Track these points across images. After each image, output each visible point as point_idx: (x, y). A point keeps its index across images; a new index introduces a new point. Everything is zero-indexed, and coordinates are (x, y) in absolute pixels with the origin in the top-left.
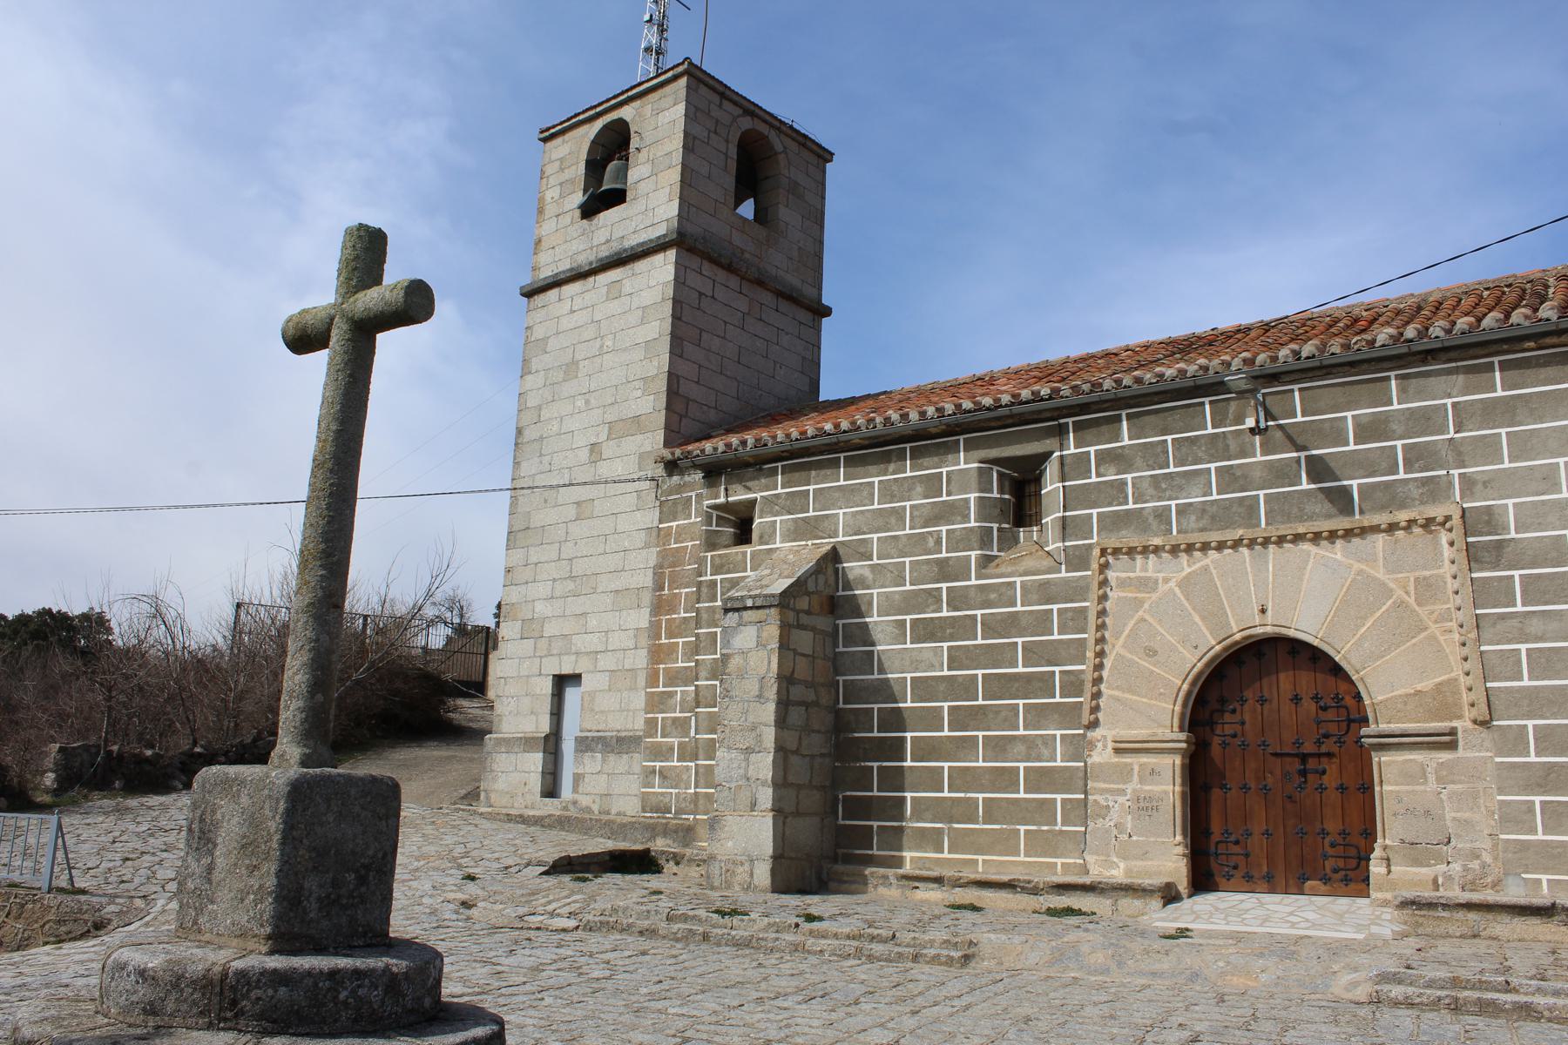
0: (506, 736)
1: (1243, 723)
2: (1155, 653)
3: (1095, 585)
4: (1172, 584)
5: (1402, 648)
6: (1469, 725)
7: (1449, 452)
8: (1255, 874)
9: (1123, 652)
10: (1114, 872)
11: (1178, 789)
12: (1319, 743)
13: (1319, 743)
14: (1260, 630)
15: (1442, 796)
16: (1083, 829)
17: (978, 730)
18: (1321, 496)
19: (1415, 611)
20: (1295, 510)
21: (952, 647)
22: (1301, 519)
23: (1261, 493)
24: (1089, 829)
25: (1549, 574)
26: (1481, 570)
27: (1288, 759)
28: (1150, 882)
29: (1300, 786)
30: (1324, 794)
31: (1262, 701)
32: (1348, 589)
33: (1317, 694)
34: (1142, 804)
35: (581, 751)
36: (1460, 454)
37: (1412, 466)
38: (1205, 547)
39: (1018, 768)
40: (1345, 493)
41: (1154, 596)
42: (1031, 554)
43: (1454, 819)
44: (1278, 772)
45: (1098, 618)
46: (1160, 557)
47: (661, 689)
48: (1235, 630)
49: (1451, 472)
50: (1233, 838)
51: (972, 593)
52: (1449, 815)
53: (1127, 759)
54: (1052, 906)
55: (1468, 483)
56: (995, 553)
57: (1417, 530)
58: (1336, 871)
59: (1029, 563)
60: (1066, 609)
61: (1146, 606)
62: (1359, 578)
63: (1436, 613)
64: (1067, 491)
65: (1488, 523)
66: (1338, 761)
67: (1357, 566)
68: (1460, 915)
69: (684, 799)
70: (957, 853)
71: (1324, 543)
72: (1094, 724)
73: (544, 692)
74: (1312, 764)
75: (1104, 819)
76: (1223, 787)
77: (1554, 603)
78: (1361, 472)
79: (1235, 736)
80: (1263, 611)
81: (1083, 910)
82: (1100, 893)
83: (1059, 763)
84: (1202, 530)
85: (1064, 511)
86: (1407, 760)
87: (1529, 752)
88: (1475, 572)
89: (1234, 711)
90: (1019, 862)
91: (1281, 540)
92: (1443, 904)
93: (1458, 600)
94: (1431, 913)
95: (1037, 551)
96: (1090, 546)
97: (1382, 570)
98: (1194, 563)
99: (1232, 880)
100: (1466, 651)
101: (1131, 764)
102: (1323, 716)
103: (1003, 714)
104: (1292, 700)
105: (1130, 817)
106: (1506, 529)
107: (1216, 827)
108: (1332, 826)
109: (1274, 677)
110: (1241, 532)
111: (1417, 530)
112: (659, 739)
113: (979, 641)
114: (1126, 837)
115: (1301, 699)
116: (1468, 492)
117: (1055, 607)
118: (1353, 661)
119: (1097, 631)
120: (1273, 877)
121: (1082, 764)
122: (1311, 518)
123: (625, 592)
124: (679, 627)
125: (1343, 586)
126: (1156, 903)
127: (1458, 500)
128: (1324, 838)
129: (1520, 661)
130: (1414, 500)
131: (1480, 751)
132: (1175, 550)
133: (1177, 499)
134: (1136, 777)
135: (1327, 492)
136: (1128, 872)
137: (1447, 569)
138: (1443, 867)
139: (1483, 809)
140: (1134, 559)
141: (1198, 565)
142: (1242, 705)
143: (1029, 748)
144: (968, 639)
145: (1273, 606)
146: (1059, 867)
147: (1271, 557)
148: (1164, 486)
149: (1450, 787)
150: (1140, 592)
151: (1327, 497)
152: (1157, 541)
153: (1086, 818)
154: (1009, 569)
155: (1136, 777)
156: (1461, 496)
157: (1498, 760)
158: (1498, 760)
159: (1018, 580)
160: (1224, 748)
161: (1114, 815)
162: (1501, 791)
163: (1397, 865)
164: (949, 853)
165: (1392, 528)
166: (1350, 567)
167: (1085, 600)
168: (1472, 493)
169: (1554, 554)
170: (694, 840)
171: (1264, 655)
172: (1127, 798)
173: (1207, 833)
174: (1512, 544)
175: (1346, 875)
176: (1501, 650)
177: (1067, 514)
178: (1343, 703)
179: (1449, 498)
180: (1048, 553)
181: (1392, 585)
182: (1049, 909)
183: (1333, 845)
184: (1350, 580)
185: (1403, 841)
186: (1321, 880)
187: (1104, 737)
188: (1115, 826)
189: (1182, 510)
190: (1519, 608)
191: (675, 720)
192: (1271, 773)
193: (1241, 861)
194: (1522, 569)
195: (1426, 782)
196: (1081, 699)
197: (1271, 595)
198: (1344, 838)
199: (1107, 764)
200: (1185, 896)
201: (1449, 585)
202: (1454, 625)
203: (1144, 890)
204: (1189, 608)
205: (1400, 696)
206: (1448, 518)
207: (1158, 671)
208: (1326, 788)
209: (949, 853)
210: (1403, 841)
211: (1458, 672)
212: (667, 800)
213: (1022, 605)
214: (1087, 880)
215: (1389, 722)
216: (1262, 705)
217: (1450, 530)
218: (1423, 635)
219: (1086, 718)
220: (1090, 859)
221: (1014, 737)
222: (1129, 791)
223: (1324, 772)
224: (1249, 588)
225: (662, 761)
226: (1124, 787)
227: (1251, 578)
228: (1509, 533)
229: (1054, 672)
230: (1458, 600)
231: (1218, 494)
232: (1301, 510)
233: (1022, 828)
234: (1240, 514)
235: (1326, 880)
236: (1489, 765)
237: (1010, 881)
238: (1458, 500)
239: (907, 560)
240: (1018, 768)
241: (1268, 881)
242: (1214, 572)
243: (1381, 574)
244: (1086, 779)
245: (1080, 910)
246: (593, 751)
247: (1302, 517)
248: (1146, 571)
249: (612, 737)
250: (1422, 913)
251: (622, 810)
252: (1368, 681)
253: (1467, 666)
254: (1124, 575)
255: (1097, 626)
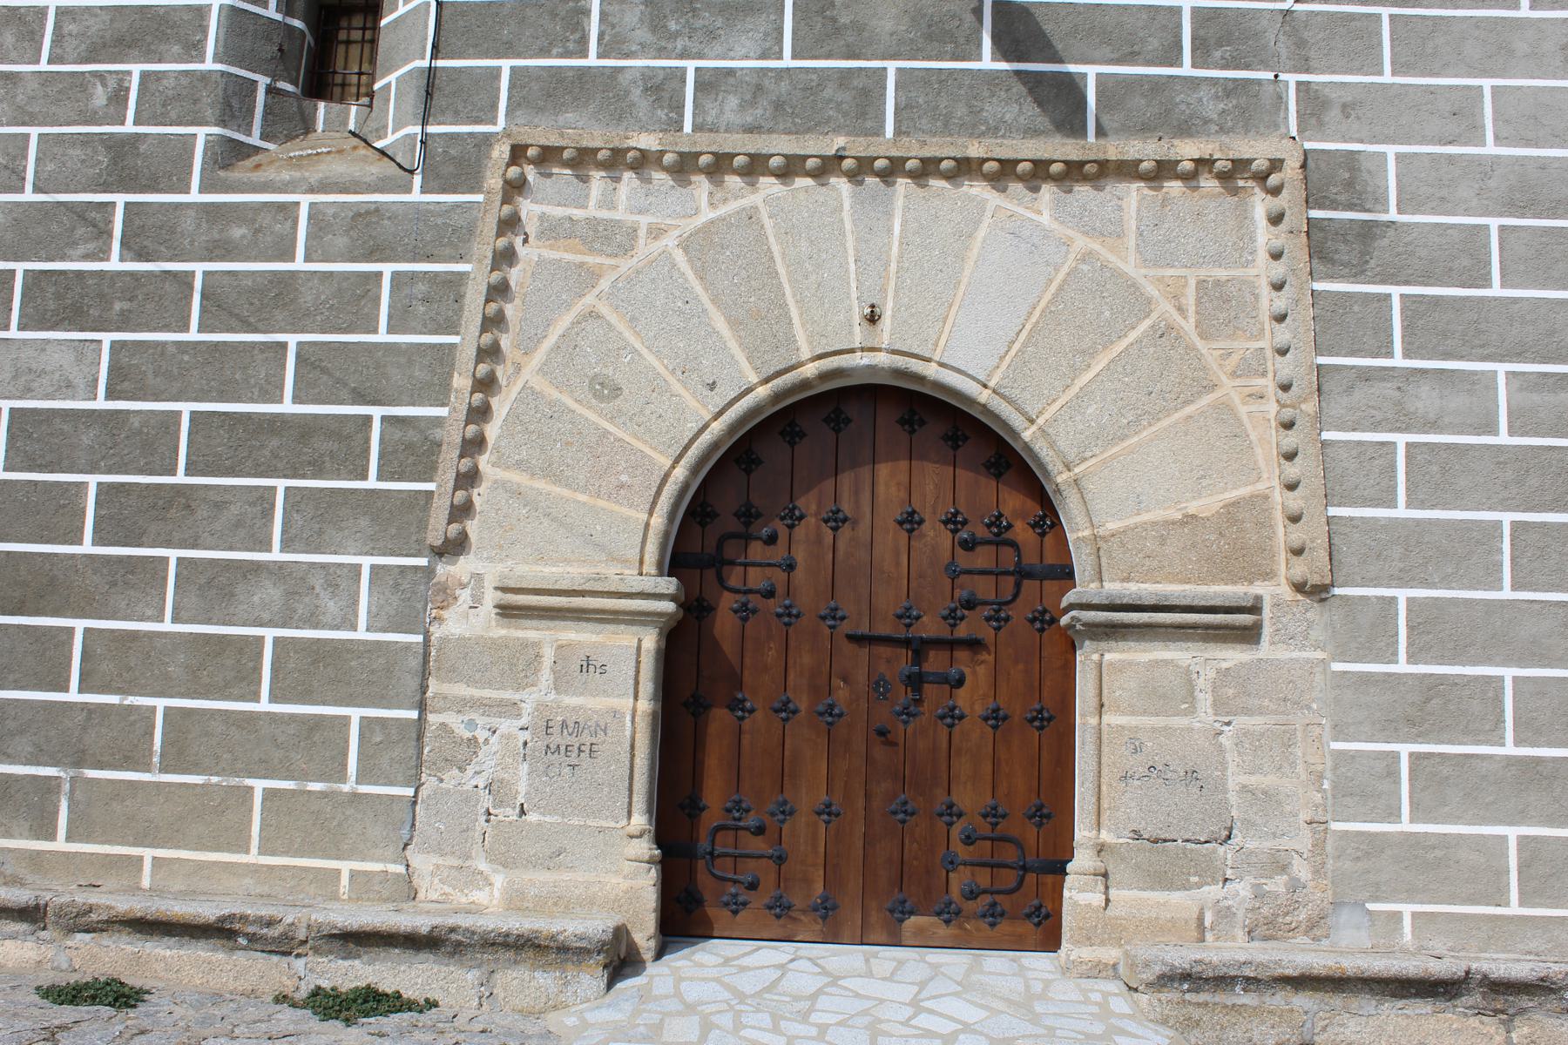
1: (791, 567)
2: (617, 391)
3: (490, 225)
4: (670, 241)
5: (1166, 422)
6: (1287, 593)
7: (1281, 37)
8: (798, 901)
9: (539, 383)
10: (480, 896)
11: (645, 705)
12: (952, 618)
13: (952, 618)
14: (861, 360)
15: (1222, 739)
16: (410, 792)
17: (168, 544)
18: (1019, 88)
19: (1195, 349)
20: (961, 111)
21: (124, 344)
22: (973, 129)
23: (892, 66)
24: (423, 792)
25: (1455, 299)
26: (1331, 277)
27: (884, 651)
28: (580, 930)
29: (906, 711)
30: (956, 729)
31: (836, 520)
32: (1061, 288)
33: (955, 514)
34: (556, 739)
36: (1301, 44)
37: (1208, 53)
38: (755, 167)
39: (261, 639)
40: (1070, 89)
41: (626, 265)
42: (340, 152)
43: (1244, 789)
44: (861, 676)
45: (487, 301)
46: (649, 181)
48: (805, 354)
49: (1282, 77)
50: (751, 821)
51: (188, 223)
52: (1235, 780)
53: (530, 632)
54: (326, 984)
55: (1314, 104)
56: (255, 140)
57: (1208, 183)
58: (972, 895)
59: (338, 168)
60: (413, 276)
61: (604, 284)
62: (1085, 267)
63: (1235, 358)
64: (446, 13)
65: (1350, 184)
66: (991, 658)
67: (1081, 243)
68: (1279, 999)
70: (88, 838)
71: (1016, 187)
72: (455, 547)
74: (935, 662)
75: (462, 769)
76: (735, 705)
77: (1461, 358)
78: (1106, 51)
79: (770, 594)
80: (873, 318)
81: (407, 994)
82: (452, 954)
83: (361, 634)
84: (751, 129)
85: (434, 56)
86: (1157, 662)
87: (1395, 653)
88: (1320, 279)
89: (772, 540)
90: (247, 865)
91: (927, 169)
92: (1247, 979)
93: (1283, 334)
94: (1221, 997)
95: (355, 148)
96: (487, 140)
97: (1132, 257)
98: (725, 200)
99: (742, 914)
100: (1291, 440)
101: (537, 644)
102: (964, 560)
103: (234, 510)
104: (901, 523)
105: (524, 768)
106: (1381, 202)
107: (714, 795)
108: (970, 798)
109: (865, 471)
110: (840, 141)
111: (1208, 183)
113: (193, 335)
114: (513, 814)
115: (921, 522)
116: (1313, 121)
117: (387, 269)
118: (1062, 444)
119: (484, 329)
120: (834, 908)
121: (420, 638)
122: (993, 131)
125: (1051, 281)
126: (590, 979)
127: (1294, 133)
128: (950, 824)
129: (1392, 467)
130: (1206, 121)
131: (1303, 648)
132: (684, 167)
133: (700, 56)
134: (546, 676)
135: (1033, 82)
136: (514, 899)
137: (1263, 270)
138: (1213, 891)
139: (1300, 768)
140: (584, 179)
141: (733, 206)
142: (791, 527)
143: (290, 594)
144: (166, 328)
145: (896, 310)
146: (345, 880)
147: (899, 202)
148: (673, 26)
149: (1241, 721)
150: (591, 251)
151: (1031, 91)
152: (647, 141)
153: (419, 766)
154: (286, 175)
155: (546, 676)
156: (1299, 126)
157: (1337, 667)
158: (1337, 667)
159: (305, 200)
160: (745, 619)
161: (487, 763)
162: (1340, 732)
163: (1120, 886)
164: (69, 839)
165: (1163, 170)
166: (1068, 245)
167: (461, 258)
168: (1321, 124)
169: (1466, 262)
171: (848, 421)
172: (524, 721)
173: (694, 807)
174: (1391, 232)
175: (994, 905)
176: (1360, 443)
177: (440, 63)
178: (1008, 535)
179: (1276, 126)
180: (382, 152)
181: (1151, 290)
182: (317, 992)
183: (968, 840)
184: (1065, 270)
185: (1137, 835)
186: (938, 914)
187: (478, 577)
188: (489, 786)
189: (708, 84)
190: (1398, 361)
192: (845, 680)
193: (766, 872)
194: (1407, 283)
195: (1192, 711)
196: (430, 486)
197: (892, 284)
198: (995, 825)
199: (479, 640)
200: (648, 956)
201: (1264, 303)
202: (1268, 384)
203: (563, 949)
204: (705, 299)
205: (1154, 524)
206: (1276, 165)
207: (620, 434)
208: (961, 717)
209: (69, 839)
210: (1137, 835)
211: (1269, 481)
213: (308, 259)
214: (421, 923)
215: (1127, 579)
216: (835, 529)
217: (1276, 191)
218: (1206, 400)
219: (438, 528)
220: (422, 862)
221: (257, 567)
222: (527, 708)
223: (960, 682)
224: (843, 266)
226: (517, 697)
227: (850, 244)
228: (1387, 211)
229: (368, 419)
230: (1283, 334)
231: (794, 57)
232: (974, 112)
233: (259, 785)
234: (839, 104)
235: (950, 914)
236: (1318, 678)
237: (222, 919)
238: (1294, 133)
239: (34, 132)
240: (261, 639)
241: (824, 918)
242: (768, 224)
243: (1130, 266)
244: (424, 674)
245: (398, 995)
247: (974, 126)
248: (612, 206)
250: (1203, 997)
252: (1090, 486)
253: (1292, 470)
254: (559, 212)
255: (485, 318)
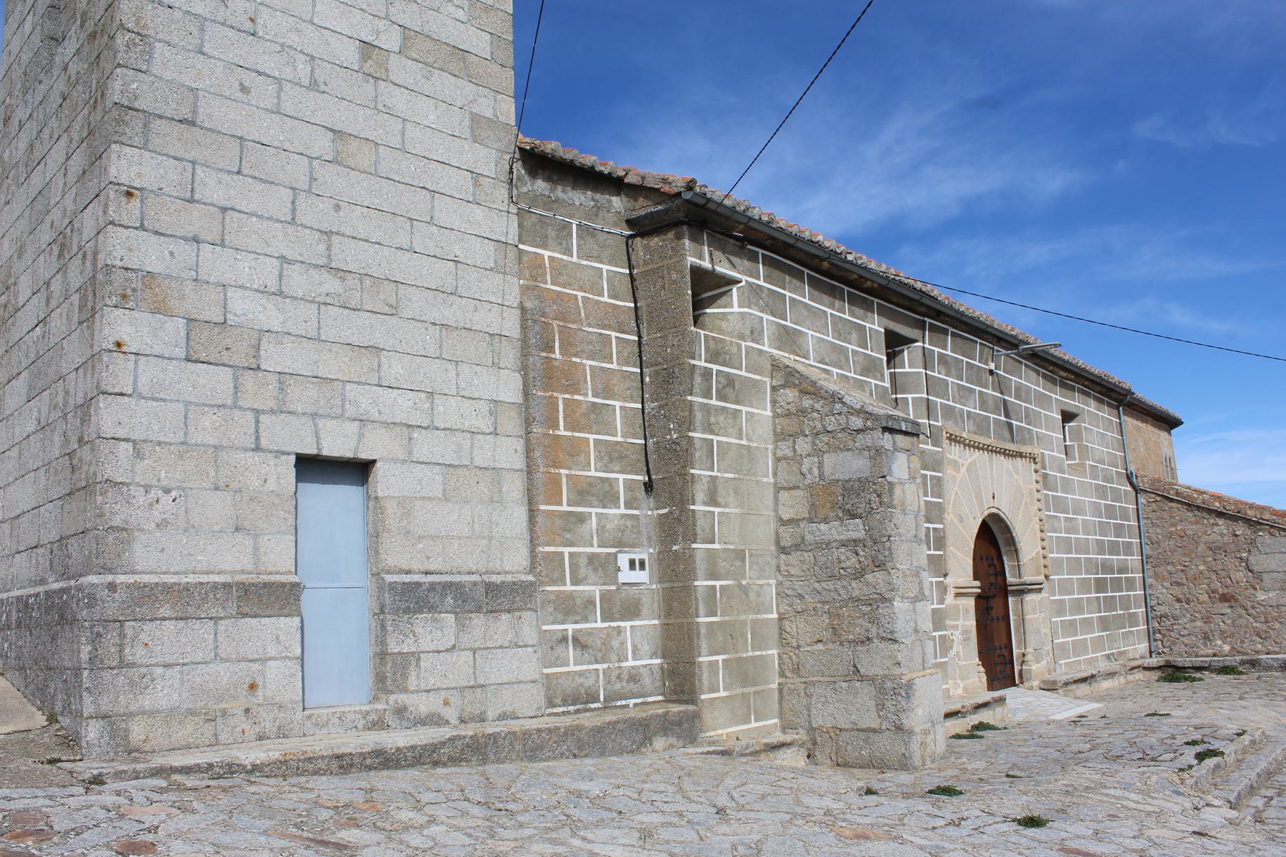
0: (146, 579)
35: (407, 611)
47: (565, 508)
69: (619, 677)
73: (272, 485)
112: (569, 587)
123: (463, 332)
124: (586, 415)
167: (939, 472)
170: (701, 731)
191: (592, 558)
212: (589, 682)
225: (576, 622)
246: (432, 609)
249: (475, 584)
251: (508, 708)
